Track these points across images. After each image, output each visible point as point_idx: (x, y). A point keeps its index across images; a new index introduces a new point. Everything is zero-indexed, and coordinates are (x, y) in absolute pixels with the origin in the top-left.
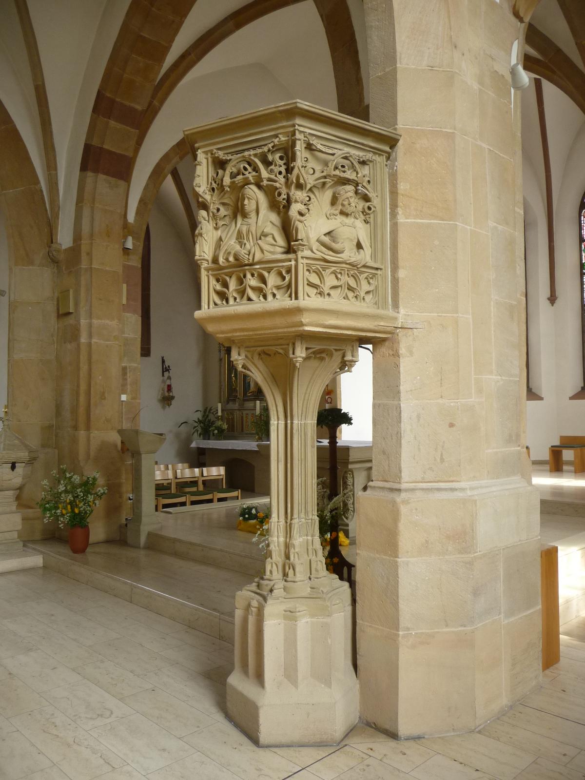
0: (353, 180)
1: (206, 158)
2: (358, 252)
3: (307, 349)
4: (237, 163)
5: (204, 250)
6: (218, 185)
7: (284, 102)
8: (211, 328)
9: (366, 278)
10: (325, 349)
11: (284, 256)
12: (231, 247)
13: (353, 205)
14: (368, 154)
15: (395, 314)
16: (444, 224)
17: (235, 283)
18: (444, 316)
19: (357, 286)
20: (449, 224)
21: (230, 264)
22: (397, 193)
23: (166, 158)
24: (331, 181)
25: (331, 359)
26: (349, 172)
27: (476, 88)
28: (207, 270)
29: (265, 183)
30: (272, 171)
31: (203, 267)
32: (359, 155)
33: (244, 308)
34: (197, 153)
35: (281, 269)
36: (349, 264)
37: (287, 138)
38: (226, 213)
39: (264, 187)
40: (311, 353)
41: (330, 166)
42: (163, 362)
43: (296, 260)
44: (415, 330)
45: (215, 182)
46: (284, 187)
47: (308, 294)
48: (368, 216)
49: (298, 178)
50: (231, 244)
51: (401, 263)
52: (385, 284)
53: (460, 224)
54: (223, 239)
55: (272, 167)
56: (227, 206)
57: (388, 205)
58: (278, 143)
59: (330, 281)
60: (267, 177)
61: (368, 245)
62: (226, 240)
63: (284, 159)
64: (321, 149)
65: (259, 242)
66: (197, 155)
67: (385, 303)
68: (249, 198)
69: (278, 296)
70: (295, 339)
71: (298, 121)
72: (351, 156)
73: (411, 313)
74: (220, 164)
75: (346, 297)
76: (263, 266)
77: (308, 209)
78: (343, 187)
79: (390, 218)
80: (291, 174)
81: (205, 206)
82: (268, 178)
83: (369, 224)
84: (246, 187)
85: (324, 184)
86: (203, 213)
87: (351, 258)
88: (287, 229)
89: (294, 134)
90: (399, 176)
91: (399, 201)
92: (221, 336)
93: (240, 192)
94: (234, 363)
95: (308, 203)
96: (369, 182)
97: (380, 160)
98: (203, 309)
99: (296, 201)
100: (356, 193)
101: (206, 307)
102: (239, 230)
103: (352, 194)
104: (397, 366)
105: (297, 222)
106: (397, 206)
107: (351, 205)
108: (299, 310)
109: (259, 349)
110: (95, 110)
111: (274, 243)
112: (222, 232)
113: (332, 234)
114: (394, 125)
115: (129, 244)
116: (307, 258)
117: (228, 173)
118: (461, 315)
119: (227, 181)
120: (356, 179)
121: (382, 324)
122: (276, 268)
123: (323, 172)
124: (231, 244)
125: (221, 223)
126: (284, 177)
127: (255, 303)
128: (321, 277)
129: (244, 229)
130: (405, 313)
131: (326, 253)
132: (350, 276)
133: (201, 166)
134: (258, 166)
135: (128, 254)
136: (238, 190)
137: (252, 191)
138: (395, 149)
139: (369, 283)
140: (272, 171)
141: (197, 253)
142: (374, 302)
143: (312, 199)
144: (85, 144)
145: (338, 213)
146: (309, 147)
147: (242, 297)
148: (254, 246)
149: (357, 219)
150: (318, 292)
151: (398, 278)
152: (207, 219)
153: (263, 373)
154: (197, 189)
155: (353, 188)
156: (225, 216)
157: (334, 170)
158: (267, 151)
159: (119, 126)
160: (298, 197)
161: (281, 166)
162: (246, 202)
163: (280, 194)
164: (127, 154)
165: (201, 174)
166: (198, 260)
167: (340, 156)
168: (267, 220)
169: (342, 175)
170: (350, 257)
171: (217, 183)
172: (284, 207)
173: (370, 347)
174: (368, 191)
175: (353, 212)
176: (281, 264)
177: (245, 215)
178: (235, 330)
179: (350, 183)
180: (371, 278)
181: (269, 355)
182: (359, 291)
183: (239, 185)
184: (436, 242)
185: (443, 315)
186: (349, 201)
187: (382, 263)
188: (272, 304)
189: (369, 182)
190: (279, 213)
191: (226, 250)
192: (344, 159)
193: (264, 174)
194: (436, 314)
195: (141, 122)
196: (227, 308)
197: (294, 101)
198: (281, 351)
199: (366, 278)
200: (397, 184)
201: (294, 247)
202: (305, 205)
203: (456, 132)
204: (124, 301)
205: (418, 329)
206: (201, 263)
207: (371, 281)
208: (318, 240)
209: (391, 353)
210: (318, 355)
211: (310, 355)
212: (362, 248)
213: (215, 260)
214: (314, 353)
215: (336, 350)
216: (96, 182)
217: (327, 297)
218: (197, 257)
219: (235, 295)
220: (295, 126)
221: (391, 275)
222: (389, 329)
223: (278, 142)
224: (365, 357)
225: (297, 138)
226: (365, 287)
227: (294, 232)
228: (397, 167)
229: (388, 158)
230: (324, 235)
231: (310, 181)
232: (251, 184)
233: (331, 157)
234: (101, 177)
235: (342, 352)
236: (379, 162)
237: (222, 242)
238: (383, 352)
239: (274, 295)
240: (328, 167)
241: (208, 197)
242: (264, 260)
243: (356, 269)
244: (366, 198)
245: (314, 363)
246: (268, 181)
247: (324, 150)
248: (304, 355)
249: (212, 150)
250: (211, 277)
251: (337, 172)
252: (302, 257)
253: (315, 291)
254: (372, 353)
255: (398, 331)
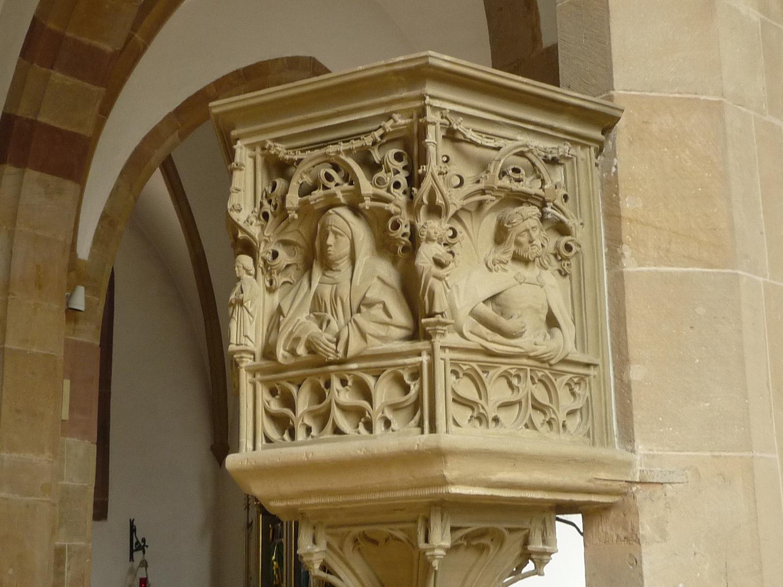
0: (536, 195)
1: (251, 157)
2: (549, 332)
3: (453, 529)
4: (314, 166)
5: (246, 333)
6: (275, 207)
7: (402, 55)
8: (259, 489)
9: (568, 384)
10: (487, 529)
11: (407, 346)
12: (302, 327)
13: (538, 242)
14: (562, 145)
15: (628, 456)
16: (713, 273)
17: (308, 397)
18: (726, 457)
19: (551, 401)
20: (724, 274)
21: (298, 360)
22: (620, 217)
23: (154, 137)
24: (494, 198)
25: (501, 547)
26: (527, 181)
27: (755, 19)
28: (253, 371)
29: (368, 204)
30: (380, 182)
31: (243, 365)
32: (545, 149)
33: (326, 448)
34: (235, 147)
35: (401, 371)
36: (535, 358)
37: (408, 121)
38: (289, 261)
39: (366, 213)
40: (461, 538)
41: (492, 171)
42: (133, 530)
43: (431, 353)
44: (668, 486)
45: (270, 202)
46: (404, 212)
47: (454, 421)
48: (566, 263)
49: (432, 195)
50: (301, 320)
51: (634, 352)
52: (605, 394)
53: (744, 274)
54: (285, 311)
55: (382, 174)
56: (292, 247)
57: (603, 239)
58: (391, 130)
59: (498, 392)
60: (371, 192)
61: (569, 319)
62: (292, 312)
63: (404, 159)
64: (476, 137)
65: (357, 317)
66: (233, 152)
67: (607, 433)
68: (335, 233)
69: (394, 425)
70: (430, 512)
71: (430, 89)
72: (530, 151)
73: (660, 453)
74: (280, 168)
75: (530, 425)
76: (364, 365)
77: (452, 253)
78: (517, 209)
79: (607, 265)
80: (419, 187)
81: (248, 248)
82: (374, 195)
83: (568, 277)
84: (330, 211)
85: (481, 204)
86: (246, 260)
87: (538, 347)
88: (413, 293)
89: (422, 113)
90: (622, 185)
91: (623, 234)
92: (279, 504)
93: (318, 221)
94: (305, 559)
95: (450, 241)
96: (566, 197)
97: (584, 155)
98: (244, 451)
99: (429, 239)
100: (542, 219)
101: (250, 446)
102: (316, 294)
103: (534, 222)
104: (637, 562)
105: (432, 280)
106: (620, 242)
107: (534, 242)
108: (439, 454)
109: (356, 530)
110: (27, 52)
111: (387, 319)
112: (283, 297)
113: (498, 299)
114: (608, 91)
115: (79, 301)
116: (452, 349)
117: (295, 185)
118: (758, 454)
119: (293, 199)
120: (541, 192)
121: (603, 475)
122: (392, 369)
123: (478, 182)
124: (301, 320)
125: (279, 280)
126: (405, 193)
127: (349, 440)
128: (478, 382)
129: (327, 292)
130: (646, 452)
131: (489, 339)
132: (536, 381)
133: (243, 172)
134: (353, 172)
135: (76, 321)
136: (315, 218)
137: (343, 219)
138: (612, 134)
139: (573, 394)
140: (380, 182)
141: (233, 339)
142: (586, 431)
143: (459, 234)
144: (3, 112)
145: (509, 259)
146: (451, 136)
147: (322, 427)
148: (348, 325)
149: (546, 269)
150: (475, 415)
151: (629, 381)
152: (253, 272)
153: (361, 576)
154: (234, 215)
155: (537, 210)
156: (288, 266)
157: (500, 178)
158: (371, 144)
159: (70, 81)
160: (432, 232)
161: (398, 172)
162: (331, 240)
163: (396, 226)
164: (81, 132)
165: (241, 187)
166: (234, 352)
167: (511, 151)
168: (374, 276)
169: (515, 186)
170: (535, 344)
171: (273, 203)
172: (405, 249)
173: (577, 519)
174: (564, 214)
175: (539, 257)
176: (400, 361)
177: (328, 266)
178: (309, 494)
179: (529, 200)
180: (576, 384)
181: (375, 542)
182: (554, 412)
183: (316, 208)
184: (701, 310)
185: (723, 454)
186: (530, 235)
187: (597, 355)
188: (383, 441)
189: (566, 197)
190: (394, 261)
191: (291, 333)
192: (520, 156)
193: (367, 187)
194: (709, 454)
195: (109, 74)
196: (294, 450)
197: (423, 54)
198: (400, 535)
199: (568, 384)
200: (619, 199)
201: (428, 328)
202: (445, 245)
203: (724, 100)
204: (65, 414)
205: (674, 485)
206: (242, 357)
207: (576, 389)
208: (473, 313)
209: (623, 534)
210: (474, 542)
211: (460, 542)
212: (558, 326)
213: (269, 353)
214: (466, 537)
215: (511, 530)
216: (21, 183)
217: (492, 424)
218: (232, 347)
219: (308, 421)
220: (424, 99)
221: (615, 377)
222: (615, 486)
223: (392, 127)
224: (568, 538)
225: (429, 120)
226: (566, 401)
227: (426, 297)
228: (616, 167)
229: (599, 152)
230: (484, 302)
231: (455, 199)
232: (341, 205)
233: (494, 153)
234: (32, 174)
235: (521, 535)
236: (582, 160)
237: (282, 318)
238: (606, 533)
239: (387, 423)
240: (488, 172)
241: (255, 230)
242: (366, 353)
243: (547, 366)
244: (561, 229)
245: (467, 557)
246: (372, 200)
247: (479, 142)
248: (447, 544)
249: (264, 142)
250: (260, 387)
251: (505, 182)
252: (441, 347)
253: (468, 413)
254: (582, 534)
255: (634, 489)
